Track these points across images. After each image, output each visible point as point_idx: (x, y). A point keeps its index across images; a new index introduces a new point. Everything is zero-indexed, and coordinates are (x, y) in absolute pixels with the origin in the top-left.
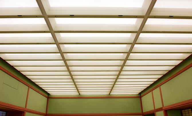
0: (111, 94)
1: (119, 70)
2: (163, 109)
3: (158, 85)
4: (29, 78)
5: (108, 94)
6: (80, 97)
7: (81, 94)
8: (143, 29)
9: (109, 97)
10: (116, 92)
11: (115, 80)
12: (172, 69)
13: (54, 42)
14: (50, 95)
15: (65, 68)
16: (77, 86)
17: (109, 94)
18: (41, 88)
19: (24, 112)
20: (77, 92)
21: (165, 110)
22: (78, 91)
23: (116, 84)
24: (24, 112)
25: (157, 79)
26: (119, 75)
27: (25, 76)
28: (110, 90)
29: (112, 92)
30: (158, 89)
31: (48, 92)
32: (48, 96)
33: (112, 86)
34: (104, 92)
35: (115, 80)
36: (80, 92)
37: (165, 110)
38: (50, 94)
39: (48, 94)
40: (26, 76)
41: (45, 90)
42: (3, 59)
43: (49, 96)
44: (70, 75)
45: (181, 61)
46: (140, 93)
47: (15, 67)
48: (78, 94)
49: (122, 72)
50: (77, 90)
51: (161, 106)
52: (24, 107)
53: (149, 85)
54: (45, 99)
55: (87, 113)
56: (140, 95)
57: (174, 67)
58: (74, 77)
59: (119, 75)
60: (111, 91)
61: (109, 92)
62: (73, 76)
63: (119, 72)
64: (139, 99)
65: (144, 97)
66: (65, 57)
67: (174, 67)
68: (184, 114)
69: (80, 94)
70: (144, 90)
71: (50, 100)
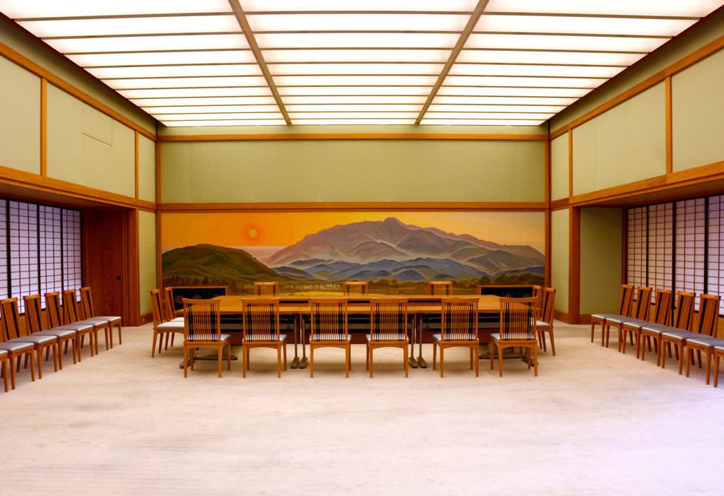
0: (423, 122)
1: (462, 29)
2: (570, 202)
3: (663, 72)
4: (126, 97)
5: (413, 122)
6: (291, 136)
7: (293, 122)
8: (477, 25)
9: (415, 136)
10: (440, 119)
11: (456, 38)
12: (634, 64)
13: (232, 11)
14: (164, 126)
15: (241, 41)
16: (279, 89)
17: (417, 124)
18: (98, 84)
19: (134, 210)
20: (281, 116)
21: (574, 208)
22: (282, 106)
23: (468, 44)
24: (134, 210)
25: (621, 70)
26: (460, 47)
27: (12, 21)
28: (421, 108)
29: (427, 115)
30: (662, 87)
31: (157, 118)
32: (158, 132)
33: (446, 55)
34: (399, 117)
35: (422, 106)
36: (291, 116)
37: (574, 208)
38: (165, 123)
39: (158, 125)
40: (87, 70)
41: (121, 93)
42: (8, 18)
43: (162, 133)
44: (234, 13)
45: (666, 40)
46: (548, 124)
47: (71, 58)
48: (284, 122)
49: (483, 18)
50: (268, 91)
51: (566, 195)
52: (133, 196)
53: (604, 81)
54: (147, 146)
55: (319, 200)
56: (549, 130)
57: (644, 55)
58: (272, 69)
59: (460, 47)
60: (425, 110)
61: (417, 115)
62: (257, 37)
63: (443, 66)
64: (540, 148)
65: (557, 139)
66: (250, 25)
67: (693, 22)
68: (680, 208)
69: (289, 124)
70: (592, 92)
71: (167, 148)
